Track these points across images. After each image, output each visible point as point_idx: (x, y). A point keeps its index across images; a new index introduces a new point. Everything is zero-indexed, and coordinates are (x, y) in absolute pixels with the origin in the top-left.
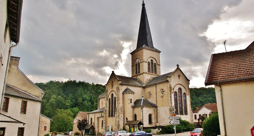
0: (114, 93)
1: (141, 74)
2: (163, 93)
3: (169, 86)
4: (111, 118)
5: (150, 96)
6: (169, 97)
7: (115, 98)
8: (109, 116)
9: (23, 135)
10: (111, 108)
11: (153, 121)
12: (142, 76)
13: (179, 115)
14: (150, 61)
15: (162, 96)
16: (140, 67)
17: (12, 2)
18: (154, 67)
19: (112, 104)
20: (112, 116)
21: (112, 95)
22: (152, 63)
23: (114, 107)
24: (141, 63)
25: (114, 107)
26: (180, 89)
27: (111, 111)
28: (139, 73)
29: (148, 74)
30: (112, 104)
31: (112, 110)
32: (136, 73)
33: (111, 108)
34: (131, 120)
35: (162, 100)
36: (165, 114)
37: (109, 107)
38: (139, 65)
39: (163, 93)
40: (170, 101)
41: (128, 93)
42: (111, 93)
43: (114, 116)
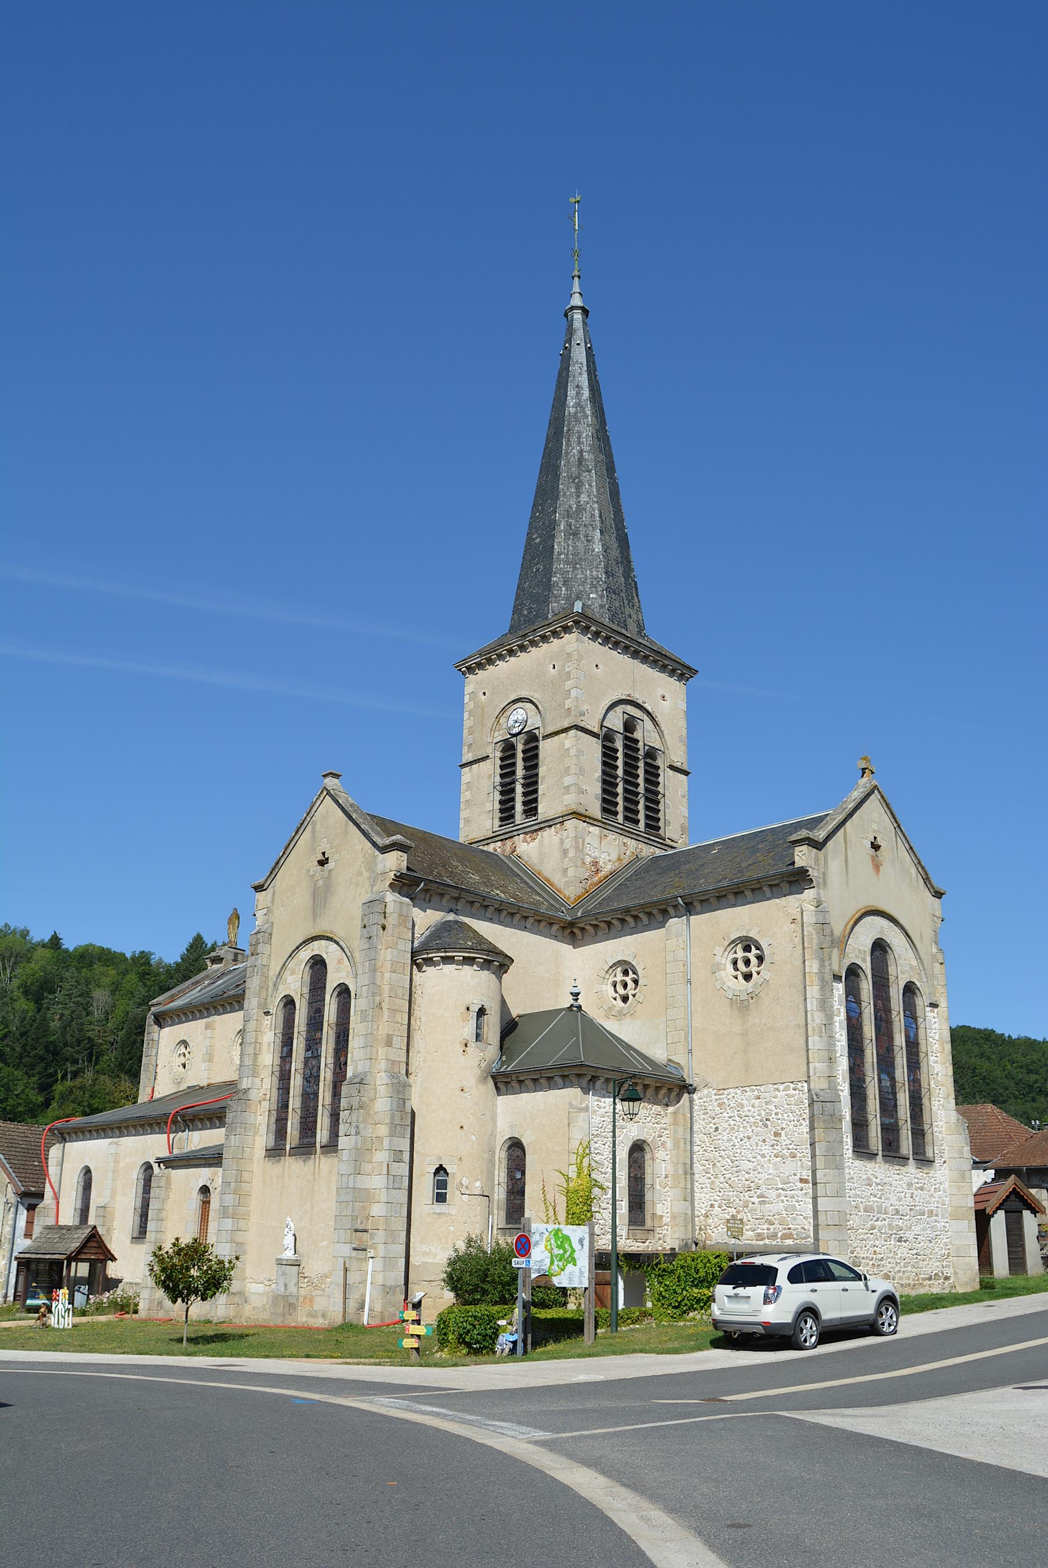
0: (328, 951)
1: (549, 823)
2: (748, 977)
3: (813, 920)
4: (292, 1166)
5: (625, 999)
6: (812, 1004)
7: (344, 991)
8: (275, 1152)
9: (1044, 1041)
10: (296, 1082)
11: (663, 1202)
12: (556, 839)
13: (880, 1158)
14: (619, 727)
15: (744, 997)
16: (542, 771)
17: (108, 1324)
18: (637, 794)
19: (313, 1044)
20: (306, 1147)
21: (318, 965)
22: (631, 744)
23: (326, 1074)
24: (545, 737)
25: (326, 1074)
26: (880, 947)
27: (295, 1102)
28: (531, 810)
29: (603, 825)
30: (313, 1044)
31: (310, 1098)
32: (506, 813)
33: (296, 1082)
34: (478, 1184)
35: (745, 1034)
36: (766, 1149)
37: (284, 1077)
38: (532, 757)
39: (748, 977)
40: (817, 1038)
41: (459, 955)
42: (305, 954)
43: (332, 1146)
